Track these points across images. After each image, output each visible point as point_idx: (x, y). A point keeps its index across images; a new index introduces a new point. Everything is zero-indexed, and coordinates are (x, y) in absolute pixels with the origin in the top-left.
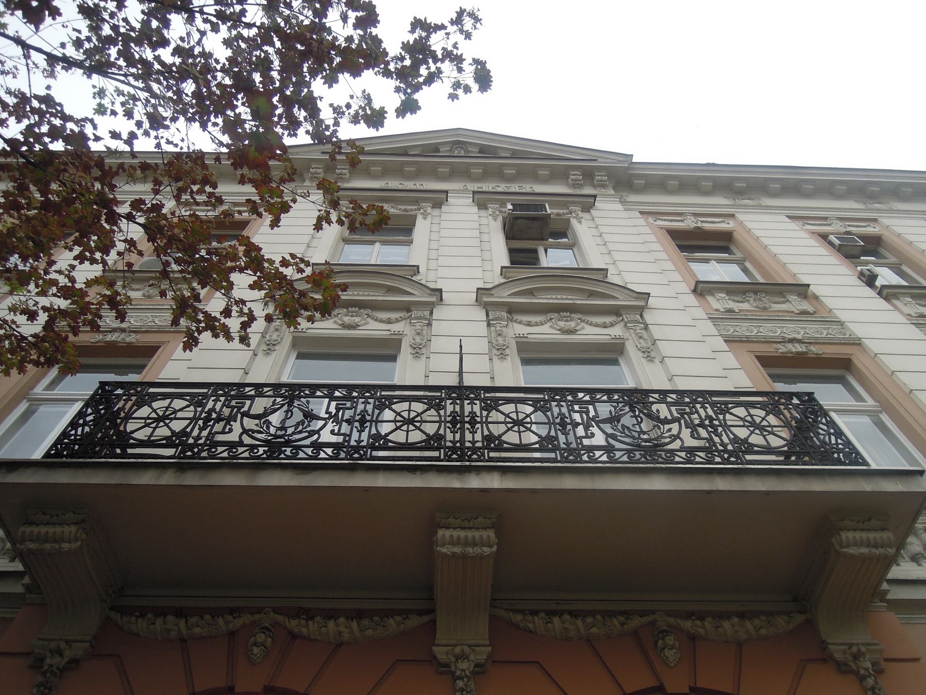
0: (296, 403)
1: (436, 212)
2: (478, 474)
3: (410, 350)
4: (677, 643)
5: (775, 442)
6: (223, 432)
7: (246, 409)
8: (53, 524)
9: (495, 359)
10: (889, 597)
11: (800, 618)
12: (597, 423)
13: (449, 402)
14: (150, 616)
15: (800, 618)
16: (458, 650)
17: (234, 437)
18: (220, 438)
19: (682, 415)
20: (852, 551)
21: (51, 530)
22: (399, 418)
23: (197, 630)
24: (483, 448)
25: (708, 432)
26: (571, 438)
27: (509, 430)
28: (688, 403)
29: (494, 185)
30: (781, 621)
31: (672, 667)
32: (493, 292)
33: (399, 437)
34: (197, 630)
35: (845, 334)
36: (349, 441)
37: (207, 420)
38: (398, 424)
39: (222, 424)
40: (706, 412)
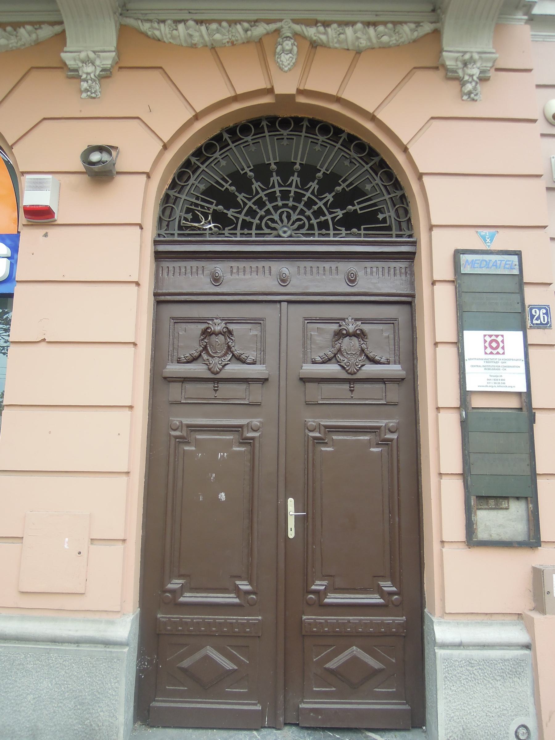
4: (295, 48)
11: (427, 28)
31: (286, 72)
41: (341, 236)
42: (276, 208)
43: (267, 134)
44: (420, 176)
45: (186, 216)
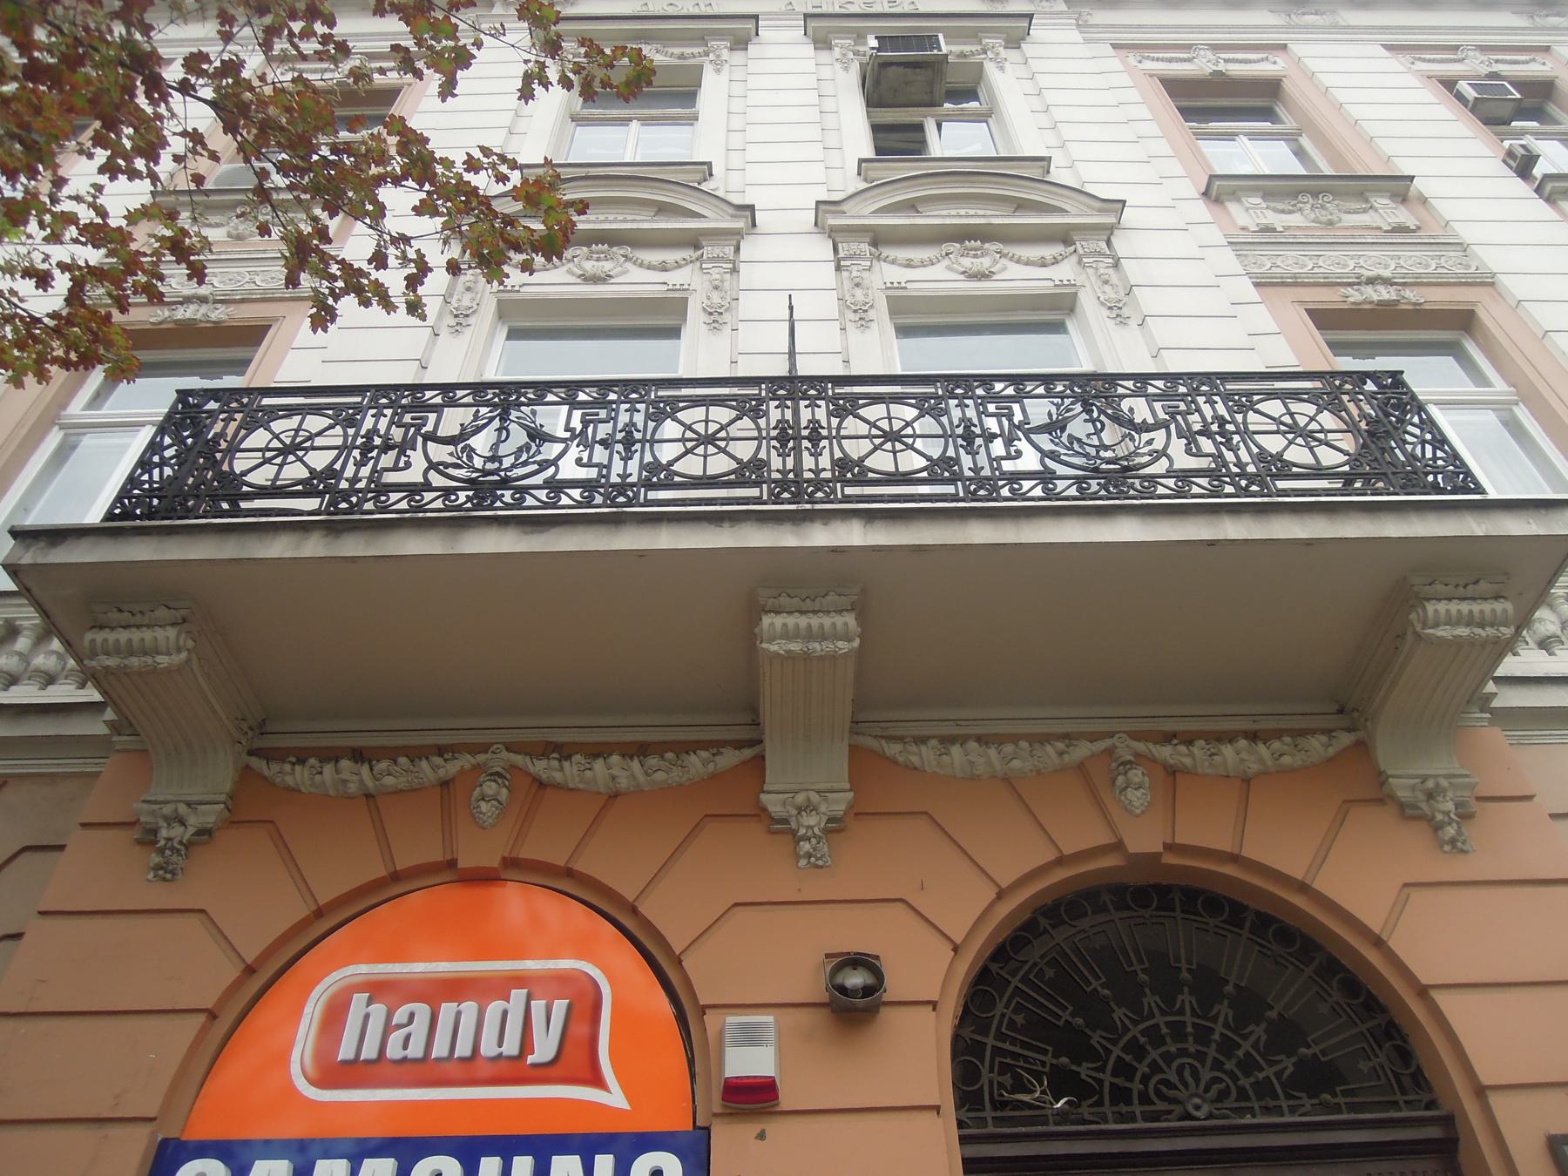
0: (514, 414)
1: (738, 57)
3: (705, 318)
5: (1329, 458)
6: (396, 469)
7: (429, 427)
9: (850, 327)
10: (1495, 704)
11: (1345, 739)
13: (773, 404)
14: (312, 761)
15: (1345, 739)
16: (800, 798)
17: (414, 475)
18: (390, 478)
19: (1173, 416)
20: (1443, 632)
22: (689, 434)
24: (834, 480)
26: (982, 459)
32: (844, 207)
33: (692, 466)
34: (389, 780)
36: (607, 477)
38: (689, 445)
39: (393, 454)
40: (1214, 409)
41: (1302, 1110)
42: (1168, 1058)
43: (1245, 933)
44: (1423, 992)
45: (1000, 1079)
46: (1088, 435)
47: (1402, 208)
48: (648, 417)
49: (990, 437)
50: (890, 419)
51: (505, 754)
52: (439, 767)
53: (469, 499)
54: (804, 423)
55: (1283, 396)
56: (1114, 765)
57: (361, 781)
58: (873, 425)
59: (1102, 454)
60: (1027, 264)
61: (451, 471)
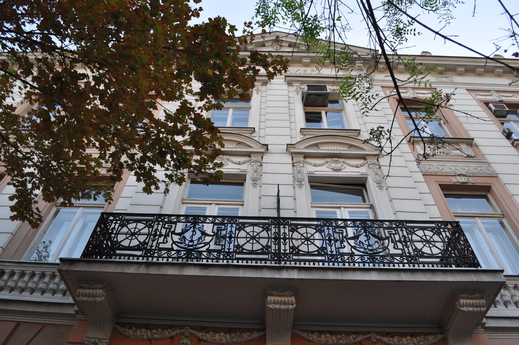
0: (197, 226)
1: (264, 88)
2: (287, 271)
3: (251, 182)
5: (435, 251)
6: (163, 243)
7: (172, 230)
8: (92, 289)
9: (296, 187)
11: (440, 337)
12: (347, 239)
13: (273, 226)
14: (134, 328)
15: (440, 337)
17: (168, 245)
18: (161, 246)
19: (390, 234)
20: (465, 309)
21: (91, 291)
22: (248, 236)
23: (156, 336)
24: (290, 253)
25: (403, 245)
26: (333, 248)
27: (303, 243)
28: (394, 228)
29: (297, 69)
30: (430, 338)
32: (296, 146)
33: (248, 247)
34: (156, 336)
35: (490, 170)
36: (224, 249)
37: (155, 235)
38: (248, 239)
39: (163, 237)
40: (403, 233)
46: (365, 241)
47: (470, 148)
48: (236, 229)
49: (336, 241)
50: (307, 233)
51: (189, 330)
52: (170, 333)
53: (184, 254)
54: (282, 234)
55: (423, 229)
56: (370, 343)
57: (148, 335)
58: (302, 235)
59: (369, 248)
60: (352, 166)
61: (179, 244)
